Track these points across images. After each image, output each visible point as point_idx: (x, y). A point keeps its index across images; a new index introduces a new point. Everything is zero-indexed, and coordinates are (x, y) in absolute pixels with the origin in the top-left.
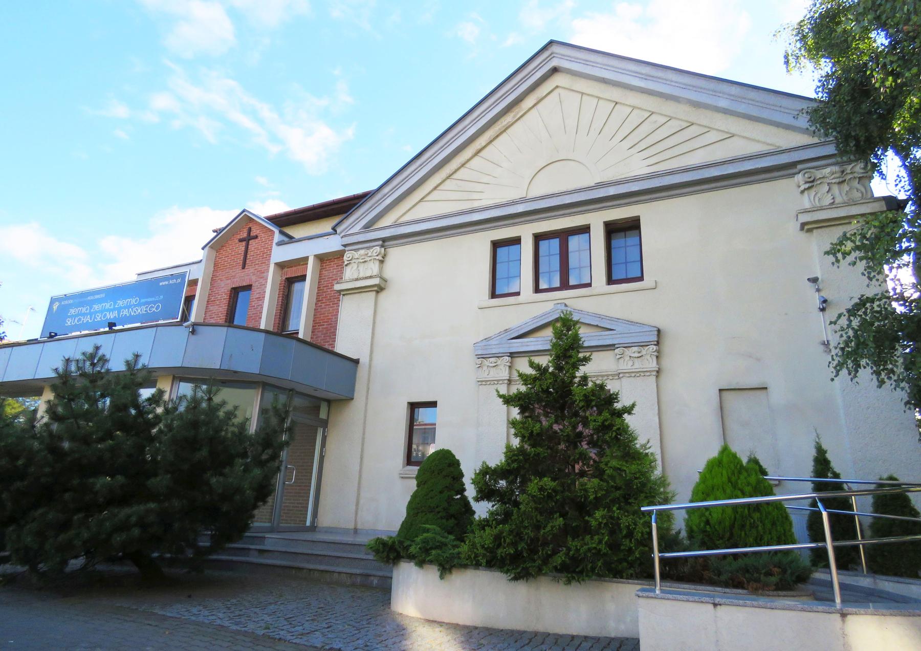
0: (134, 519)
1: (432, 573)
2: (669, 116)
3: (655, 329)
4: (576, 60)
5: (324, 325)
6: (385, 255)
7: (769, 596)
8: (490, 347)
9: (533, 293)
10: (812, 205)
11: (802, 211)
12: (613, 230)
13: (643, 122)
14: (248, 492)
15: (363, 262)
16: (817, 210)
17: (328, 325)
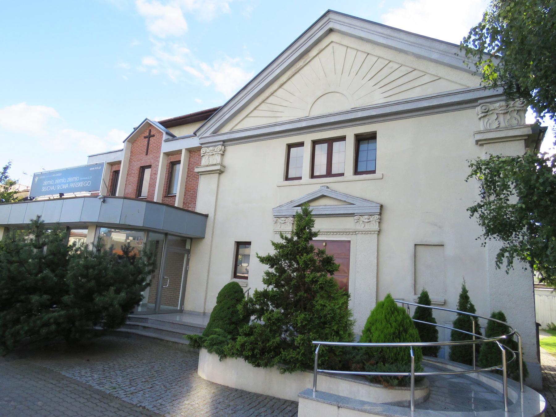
0: (52, 320)
1: (216, 357)
2: (401, 64)
3: (379, 205)
4: (343, 24)
5: (191, 192)
6: (225, 151)
7: (396, 389)
8: (282, 211)
9: (310, 178)
10: (485, 128)
11: (477, 132)
12: (360, 139)
13: (384, 67)
14: (117, 306)
15: (211, 155)
16: (487, 132)
17: (193, 191)
